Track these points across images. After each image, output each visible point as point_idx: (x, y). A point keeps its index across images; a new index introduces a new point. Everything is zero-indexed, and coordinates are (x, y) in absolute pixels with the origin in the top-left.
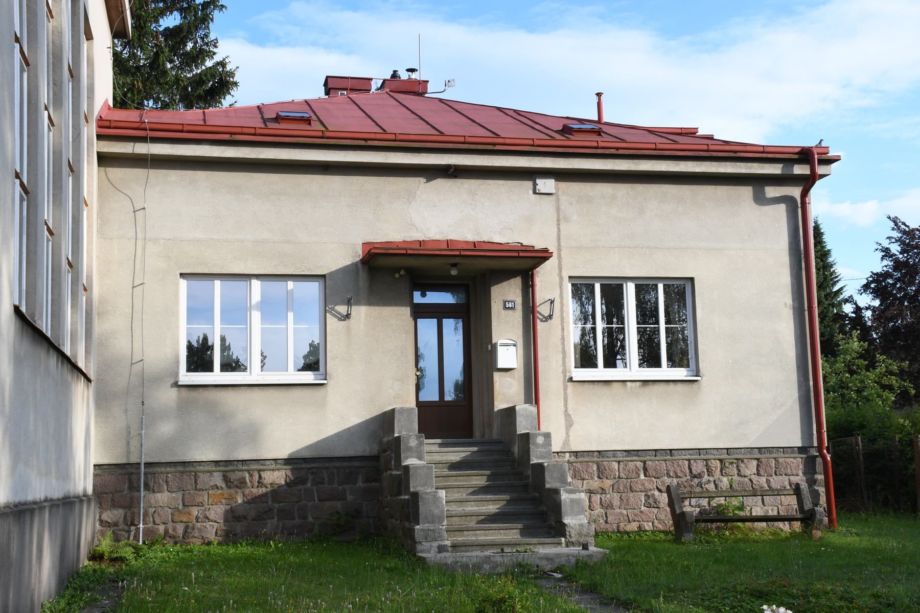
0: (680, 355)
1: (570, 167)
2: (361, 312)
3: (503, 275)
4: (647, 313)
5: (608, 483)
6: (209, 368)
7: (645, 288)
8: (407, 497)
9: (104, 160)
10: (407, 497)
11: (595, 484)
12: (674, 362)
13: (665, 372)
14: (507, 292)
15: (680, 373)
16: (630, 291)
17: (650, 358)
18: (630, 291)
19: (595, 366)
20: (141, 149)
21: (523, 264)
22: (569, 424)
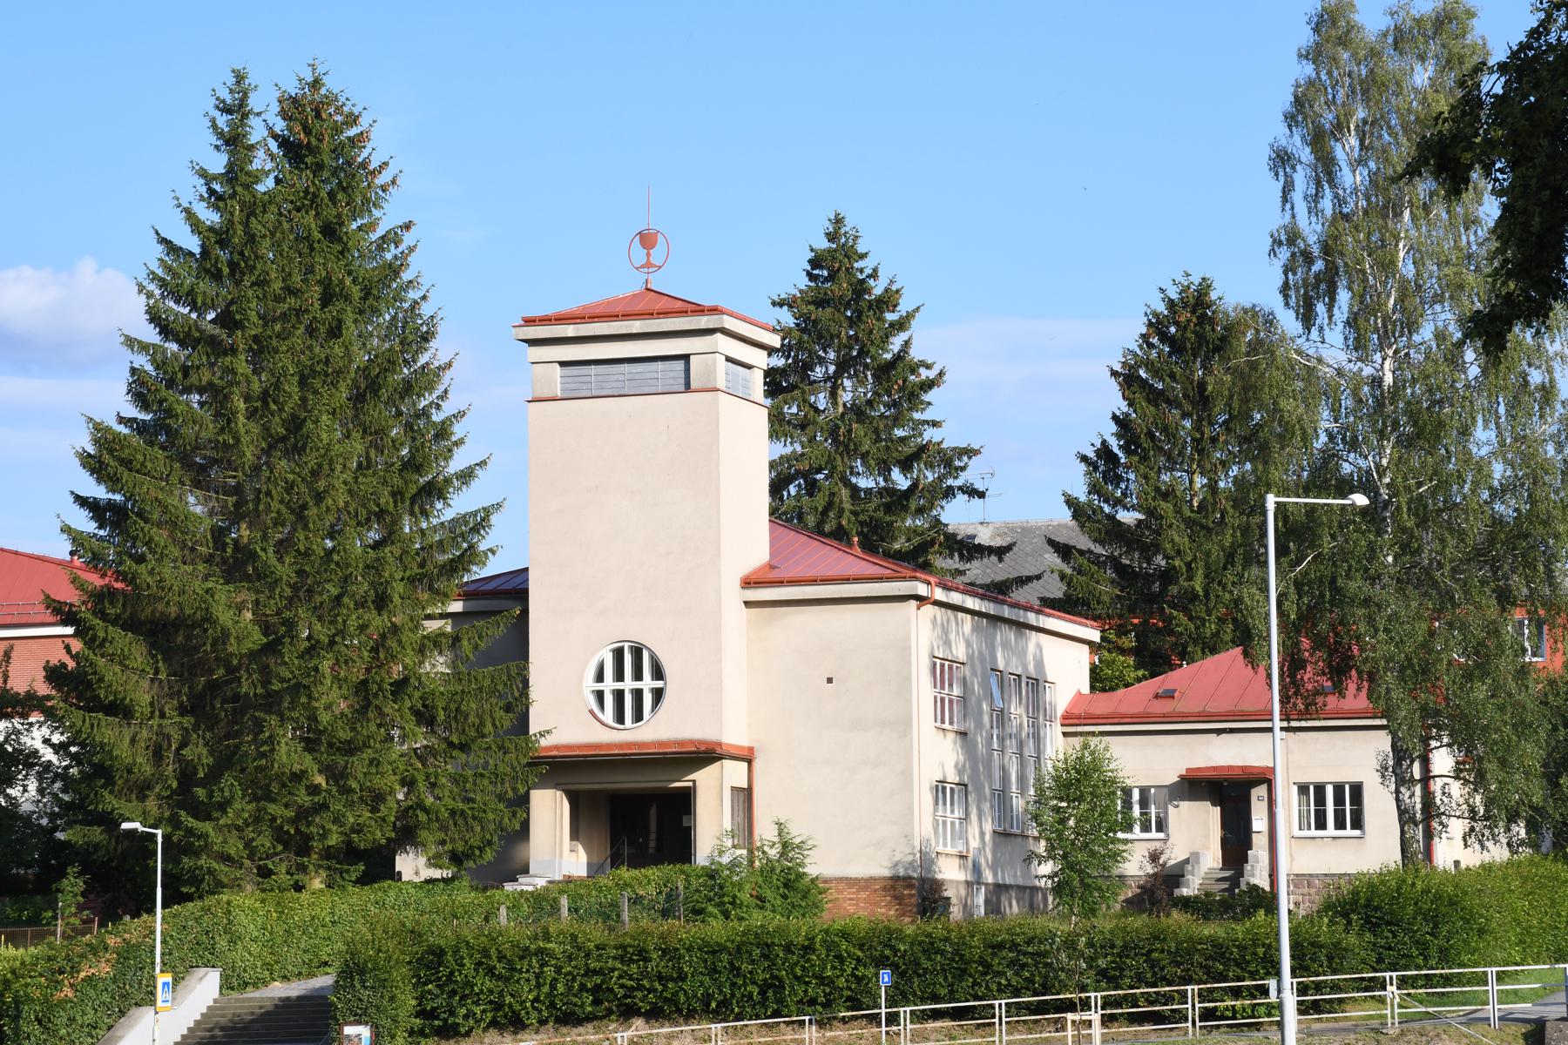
0: (1358, 823)
1: (1238, 761)
2: (1185, 805)
3: (1257, 782)
4: (1339, 800)
5: (1313, 891)
6: (1344, 828)
7: (1339, 789)
8: (407, 530)
9: (1065, 734)
10: (407, 530)
11: (1306, 890)
12: (1353, 827)
13: (1349, 832)
14: (1259, 792)
15: (1357, 833)
16: (1330, 791)
17: (1340, 825)
18: (1330, 791)
19: (1344, 828)
20: (1080, 729)
21: (1264, 778)
22: (1292, 859)
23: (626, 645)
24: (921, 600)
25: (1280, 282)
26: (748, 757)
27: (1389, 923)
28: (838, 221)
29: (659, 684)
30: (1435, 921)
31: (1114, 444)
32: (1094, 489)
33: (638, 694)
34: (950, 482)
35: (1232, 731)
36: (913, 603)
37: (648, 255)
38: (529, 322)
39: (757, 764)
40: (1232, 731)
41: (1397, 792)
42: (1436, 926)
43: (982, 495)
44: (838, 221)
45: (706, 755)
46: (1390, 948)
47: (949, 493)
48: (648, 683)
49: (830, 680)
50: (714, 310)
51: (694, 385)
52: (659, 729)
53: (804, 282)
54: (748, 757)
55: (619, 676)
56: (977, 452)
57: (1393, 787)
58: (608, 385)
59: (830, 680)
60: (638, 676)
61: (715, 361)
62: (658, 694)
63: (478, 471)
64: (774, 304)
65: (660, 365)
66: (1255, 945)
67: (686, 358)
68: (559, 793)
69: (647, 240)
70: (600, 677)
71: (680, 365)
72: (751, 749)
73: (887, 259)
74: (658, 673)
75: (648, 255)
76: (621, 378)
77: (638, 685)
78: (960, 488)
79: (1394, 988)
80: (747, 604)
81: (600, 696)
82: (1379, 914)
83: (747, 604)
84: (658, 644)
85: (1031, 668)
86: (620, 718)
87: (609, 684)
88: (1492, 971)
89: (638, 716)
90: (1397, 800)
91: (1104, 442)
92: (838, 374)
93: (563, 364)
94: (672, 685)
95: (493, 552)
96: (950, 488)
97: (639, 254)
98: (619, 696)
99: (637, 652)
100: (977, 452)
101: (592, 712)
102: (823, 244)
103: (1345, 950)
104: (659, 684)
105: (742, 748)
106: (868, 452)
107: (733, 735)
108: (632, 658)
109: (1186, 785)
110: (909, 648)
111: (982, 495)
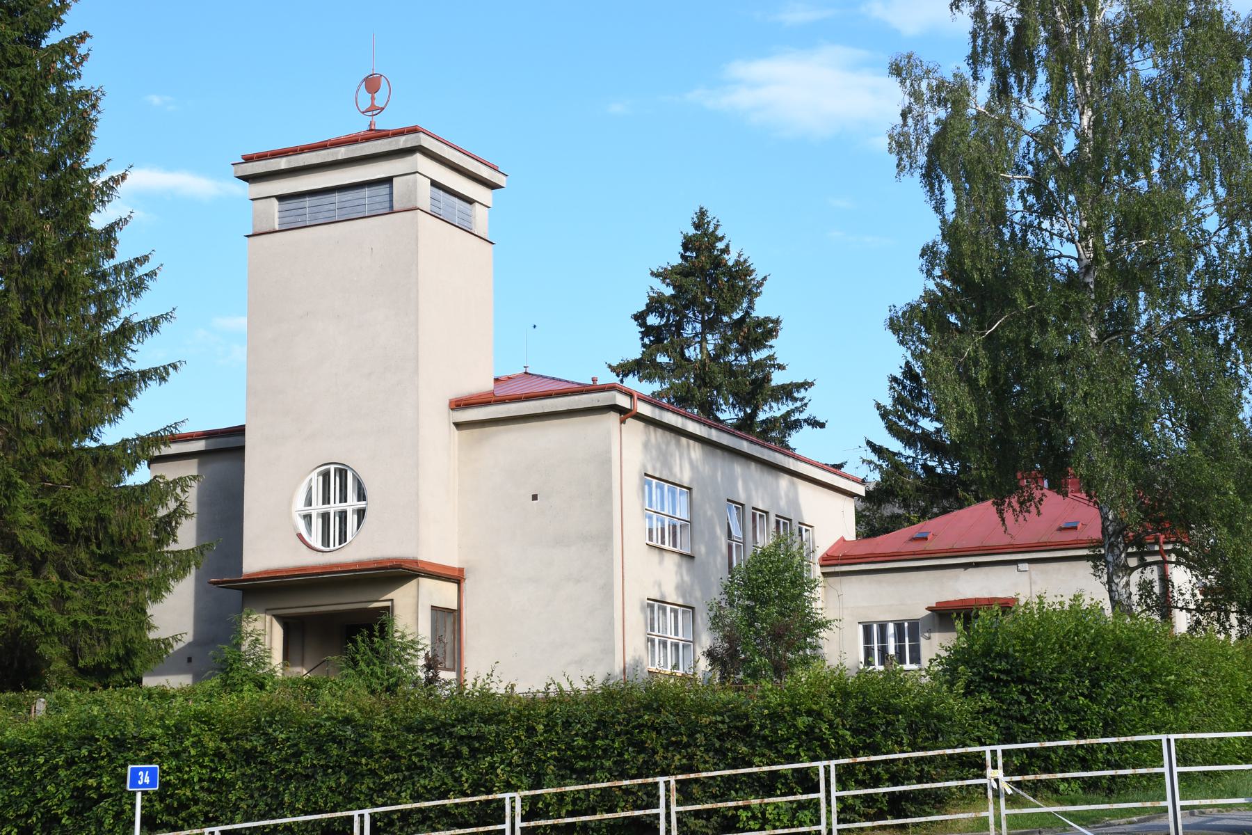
23: (332, 467)
24: (621, 411)
25: (969, 51)
26: (456, 577)
27: (1021, 680)
28: (702, 213)
29: (362, 504)
30: (1096, 676)
31: (918, 368)
32: (899, 400)
33: (343, 516)
34: (797, 416)
35: (978, 565)
36: (614, 417)
37: (373, 98)
38: (249, 159)
39: (467, 585)
40: (978, 565)
41: (1110, 581)
42: (1095, 684)
43: (822, 425)
44: (702, 213)
45: (399, 573)
46: (1023, 720)
47: (797, 425)
48: (352, 503)
49: (535, 497)
50: (414, 130)
51: (396, 207)
52: (363, 547)
53: (677, 261)
54: (456, 577)
55: (326, 500)
56: (811, 384)
57: (1105, 578)
58: (321, 216)
59: (535, 497)
60: (343, 498)
61: (415, 182)
62: (361, 513)
63: (149, 282)
64: (652, 274)
65: (366, 192)
66: (796, 712)
67: (388, 181)
68: (268, 618)
69: (372, 84)
70: (309, 502)
71: (384, 190)
72: (461, 570)
73: (739, 244)
74: (361, 496)
75: (373, 98)
76: (332, 207)
77: (342, 506)
78: (805, 421)
79: (999, 773)
80: (458, 425)
81: (308, 517)
82: (1004, 665)
83: (458, 425)
84: (360, 465)
85: (783, 503)
86: (326, 541)
87: (318, 507)
88: (1168, 740)
89: (343, 537)
90: (1110, 591)
91: (907, 363)
92: (703, 333)
93: (281, 198)
94: (371, 505)
95: (175, 367)
96: (797, 421)
97: (365, 99)
98: (325, 517)
99: (342, 473)
100: (811, 384)
101: (300, 536)
102: (691, 231)
103: (940, 718)
104: (362, 504)
105: (453, 569)
106: (721, 384)
107: (430, 554)
108: (337, 478)
109: (937, 619)
110: (608, 461)
111: (822, 425)
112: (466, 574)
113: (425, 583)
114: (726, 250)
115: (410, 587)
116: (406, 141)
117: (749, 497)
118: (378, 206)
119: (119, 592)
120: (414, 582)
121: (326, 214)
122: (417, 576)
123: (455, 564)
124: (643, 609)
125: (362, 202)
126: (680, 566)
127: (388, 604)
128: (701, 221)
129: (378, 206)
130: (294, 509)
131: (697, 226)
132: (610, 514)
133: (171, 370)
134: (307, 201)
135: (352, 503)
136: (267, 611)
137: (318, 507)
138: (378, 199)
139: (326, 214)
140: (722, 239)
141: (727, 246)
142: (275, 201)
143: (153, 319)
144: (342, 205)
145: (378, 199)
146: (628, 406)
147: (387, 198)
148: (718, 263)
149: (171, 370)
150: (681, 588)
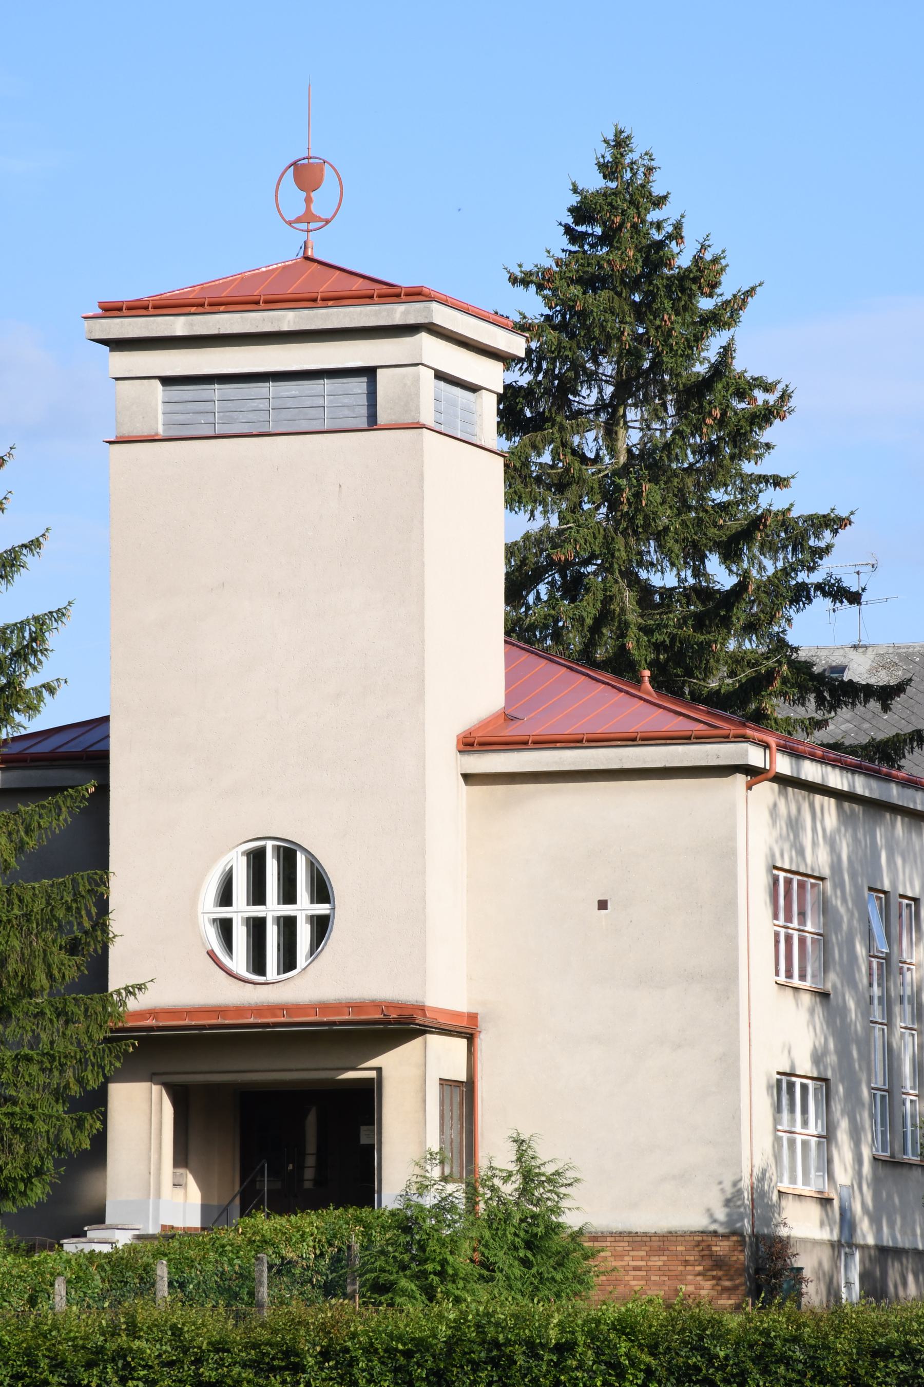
23: (269, 845)
26: (467, 1031)
28: (620, 143)
29: (322, 909)
33: (288, 925)
34: (802, 577)
36: (741, 779)
37: (308, 200)
38: (111, 310)
39: (483, 1042)
43: (855, 598)
44: (620, 143)
45: (399, 1026)
47: (801, 595)
48: (304, 908)
54: (467, 1031)
55: (258, 896)
58: (241, 417)
59: (603, 905)
60: (288, 895)
61: (417, 380)
62: (321, 926)
64: (514, 280)
65: (327, 385)
67: (369, 373)
68: (156, 1088)
69: (306, 175)
70: (225, 898)
71: (359, 385)
72: (473, 1017)
73: (698, 212)
75: (308, 200)
77: (287, 910)
78: (819, 587)
81: (225, 927)
86: (258, 964)
87: (241, 909)
89: (288, 962)
93: (167, 381)
95: (51, 690)
96: (803, 587)
97: (293, 199)
98: (257, 927)
99: (287, 856)
101: (211, 955)
102: (595, 182)
104: (322, 909)
107: (443, 995)
108: (278, 865)
110: (733, 853)
111: (855, 598)
112: (482, 1024)
113: (434, 1040)
114: (677, 234)
115: (409, 1050)
116: (406, 313)
117: (894, 883)
118: (346, 412)
119: (34, 1069)
120: (417, 1042)
121: (252, 416)
122: (422, 1031)
123: (462, 1007)
124: (770, 1087)
125: (319, 401)
126: (812, 1011)
127: (373, 1074)
128: (617, 157)
129: (346, 412)
130: (200, 910)
131: (609, 170)
132: (734, 938)
133: (45, 694)
134: (217, 391)
135: (304, 908)
136: (152, 1077)
137: (241, 909)
138: (346, 400)
139: (252, 416)
140: (659, 202)
141: (678, 227)
142: (157, 383)
143: (36, 619)
144: (278, 403)
145: (346, 400)
146: (761, 765)
147: (363, 400)
148: (655, 255)
149: (45, 694)
150: (818, 1058)
